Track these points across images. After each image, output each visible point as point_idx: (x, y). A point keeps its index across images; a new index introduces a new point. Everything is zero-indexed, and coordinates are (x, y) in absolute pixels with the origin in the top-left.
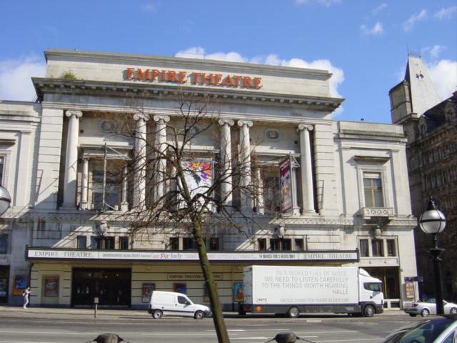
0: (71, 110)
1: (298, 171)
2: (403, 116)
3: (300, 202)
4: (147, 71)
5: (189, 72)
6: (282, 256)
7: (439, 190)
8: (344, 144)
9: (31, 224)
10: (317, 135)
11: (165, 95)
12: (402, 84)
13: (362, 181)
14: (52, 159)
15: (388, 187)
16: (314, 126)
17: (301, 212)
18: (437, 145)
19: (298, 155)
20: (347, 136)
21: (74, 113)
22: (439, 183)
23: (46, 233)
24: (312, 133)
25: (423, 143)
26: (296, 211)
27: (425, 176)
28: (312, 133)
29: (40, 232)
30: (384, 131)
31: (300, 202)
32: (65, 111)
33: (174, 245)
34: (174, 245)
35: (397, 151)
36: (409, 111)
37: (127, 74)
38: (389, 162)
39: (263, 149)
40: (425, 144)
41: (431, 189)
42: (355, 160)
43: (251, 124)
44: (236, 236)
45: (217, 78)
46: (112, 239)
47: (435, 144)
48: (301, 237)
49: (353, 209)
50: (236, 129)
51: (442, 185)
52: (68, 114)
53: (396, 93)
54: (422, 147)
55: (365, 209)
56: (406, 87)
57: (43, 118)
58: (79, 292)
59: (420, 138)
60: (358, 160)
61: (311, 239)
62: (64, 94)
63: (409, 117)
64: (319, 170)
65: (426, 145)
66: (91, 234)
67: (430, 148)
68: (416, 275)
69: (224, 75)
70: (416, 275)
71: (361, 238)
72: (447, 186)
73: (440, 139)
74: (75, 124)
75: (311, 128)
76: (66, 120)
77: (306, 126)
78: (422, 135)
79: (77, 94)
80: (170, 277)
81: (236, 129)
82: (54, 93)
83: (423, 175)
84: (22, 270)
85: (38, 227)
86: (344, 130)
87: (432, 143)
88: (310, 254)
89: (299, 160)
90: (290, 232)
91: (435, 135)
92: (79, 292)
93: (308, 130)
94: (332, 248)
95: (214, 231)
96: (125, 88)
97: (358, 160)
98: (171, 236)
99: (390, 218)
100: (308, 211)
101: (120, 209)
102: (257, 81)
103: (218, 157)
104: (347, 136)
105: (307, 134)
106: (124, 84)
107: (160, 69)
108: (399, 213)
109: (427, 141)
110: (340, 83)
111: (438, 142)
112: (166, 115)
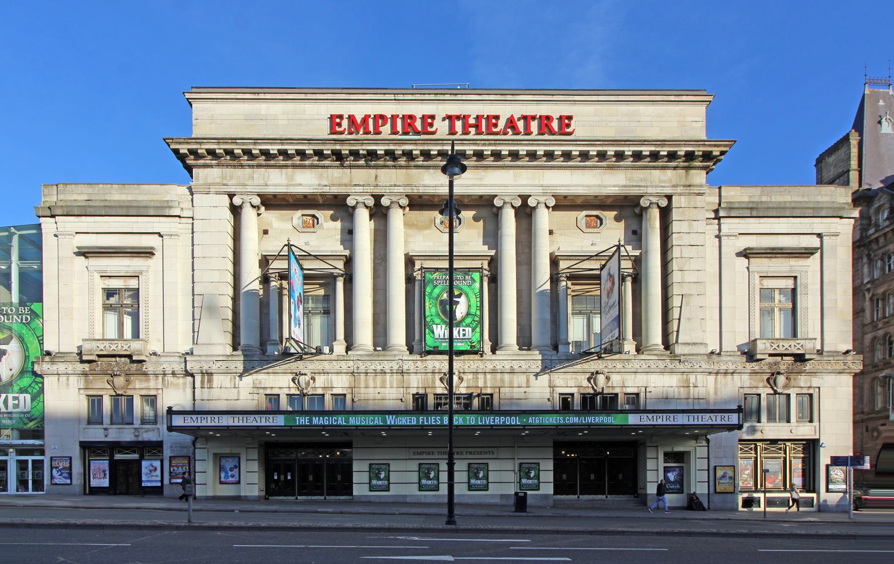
0: (242, 193)
3: (638, 333)
4: (366, 119)
8: (728, 226)
10: (675, 215)
12: (846, 139)
13: (757, 297)
15: (809, 303)
16: (669, 198)
21: (247, 198)
24: (665, 213)
25: (877, 239)
29: (206, 390)
31: (638, 333)
35: (836, 235)
38: (818, 255)
40: (882, 240)
41: (884, 317)
43: (552, 202)
44: (523, 390)
49: (736, 337)
52: (237, 201)
54: (874, 246)
55: (758, 342)
57: (196, 210)
58: (276, 478)
66: (287, 391)
75: (664, 203)
76: (236, 211)
77: (654, 200)
78: (877, 225)
80: (414, 453)
83: (868, 296)
84: (182, 447)
85: (202, 382)
88: (650, 416)
92: (276, 478)
93: (659, 207)
97: (84, 253)
98: (414, 391)
99: (807, 357)
100: (649, 350)
101: (331, 350)
105: (655, 214)
108: (825, 349)
109: (885, 235)
110: (828, 503)
112: (401, 194)
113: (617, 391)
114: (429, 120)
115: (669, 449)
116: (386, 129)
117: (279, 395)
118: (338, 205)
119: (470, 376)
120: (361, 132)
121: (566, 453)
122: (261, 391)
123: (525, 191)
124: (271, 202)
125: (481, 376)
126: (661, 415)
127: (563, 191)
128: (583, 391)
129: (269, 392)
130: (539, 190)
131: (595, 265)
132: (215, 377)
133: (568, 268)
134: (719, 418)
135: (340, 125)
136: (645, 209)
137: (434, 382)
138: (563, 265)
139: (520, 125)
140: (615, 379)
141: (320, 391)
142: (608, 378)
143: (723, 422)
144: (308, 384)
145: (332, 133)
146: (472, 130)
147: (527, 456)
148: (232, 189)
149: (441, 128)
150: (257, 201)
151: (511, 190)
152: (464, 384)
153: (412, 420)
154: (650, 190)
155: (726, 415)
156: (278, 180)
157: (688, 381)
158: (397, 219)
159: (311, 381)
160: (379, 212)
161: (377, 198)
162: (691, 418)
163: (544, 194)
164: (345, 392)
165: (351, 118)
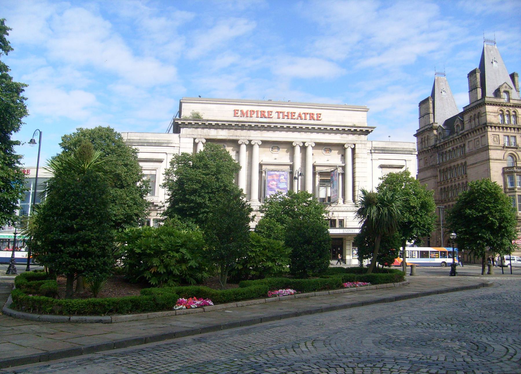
1: (344, 175)
2: (427, 124)
5: (275, 109)
7: (448, 182)
10: (357, 151)
12: (427, 100)
16: (355, 145)
17: (344, 202)
18: (448, 149)
19: (343, 165)
21: (200, 140)
22: (449, 177)
24: (353, 150)
26: (341, 201)
27: (440, 171)
28: (353, 150)
30: (402, 147)
32: (194, 139)
36: (432, 120)
37: (236, 112)
45: (293, 114)
46: (335, 220)
47: (447, 148)
50: (304, 148)
51: (451, 178)
52: (197, 141)
53: (424, 106)
56: (431, 102)
59: (438, 142)
63: (431, 126)
64: (357, 175)
65: (441, 149)
67: (444, 151)
69: (297, 111)
72: (453, 180)
73: (450, 145)
75: (353, 147)
81: (304, 148)
83: (438, 170)
86: (374, 147)
87: (446, 147)
89: (344, 168)
90: (336, 214)
91: (456, 138)
94: (361, 300)
102: (319, 115)
103: (292, 167)
104: (376, 152)
107: (255, 108)
111: (449, 147)
114: (270, 113)
116: (255, 115)
130: (309, 140)
136: (239, 146)
139: (303, 116)
142: (333, 214)
148: (195, 137)
149: (275, 115)
154: (242, 138)
158: (256, 149)
160: (250, 147)
163: (311, 142)
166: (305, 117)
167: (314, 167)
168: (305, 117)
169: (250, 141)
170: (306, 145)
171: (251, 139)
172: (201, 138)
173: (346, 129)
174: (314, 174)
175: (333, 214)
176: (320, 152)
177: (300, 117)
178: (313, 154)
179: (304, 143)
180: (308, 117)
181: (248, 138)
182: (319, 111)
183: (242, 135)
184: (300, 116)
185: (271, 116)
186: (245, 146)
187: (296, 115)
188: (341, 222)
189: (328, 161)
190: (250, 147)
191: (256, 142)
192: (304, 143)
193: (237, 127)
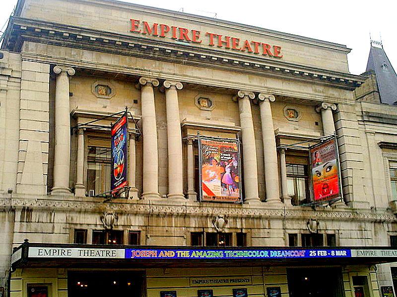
4: (155, 25)
6: (235, 254)
9: (11, 214)
11: (178, 57)
14: (39, 126)
20: (371, 119)
23: (33, 226)
26: (134, 195)
33: (80, 238)
34: (80, 238)
37: (134, 24)
39: (288, 128)
42: (381, 147)
44: (266, 231)
46: (121, 233)
48: (332, 232)
52: (57, 70)
60: (384, 146)
61: (344, 234)
62: (52, 43)
66: (93, 227)
68: (29, 257)
70: (29, 257)
71: (391, 234)
74: (63, 83)
76: (54, 78)
79: (68, 46)
81: (256, 103)
82: (39, 41)
85: (22, 217)
95: (242, 224)
96: (132, 43)
97: (384, 146)
98: (193, 230)
104: (371, 119)
106: (131, 38)
113: (323, 232)
115: (355, 275)
117: (87, 230)
118: (233, 96)
119: (231, 220)
120: (151, 35)
121: (81, 284)
122: (73, 226)
123: (257, 90)
124: (83, 74)
125: (239, 220)
126: (57, 249)
127: (279, 93)
128: (302, 232)
129: (78, 227)
131: (108, 124)
132: (33, 214)
133: (86, 124)
134: (105, 253)
135: (137, 27)
136: (239, 99)
137: (207, 224)
138: (81, 121)
139: (252, 48)
140: (322, 225)
141: (121, 228)
142: (318, 224)
143: (63, 256)
144: (112, 222)
145: (132, 32)
146: (224, 46)
147: (273, 282)
150: (273, 99)
151: (247, 88)
152: (227, 226)
153: (289, 254)
154: (147, 73)
155: (66, 249)
156: (89, 59)
157: (360, 226)
158: (172, 98)
159: (115, 220)
160: (256, 103)
161: (162, 81)
162: (82, 253)
163: (268, 93)
164: (140, 229)
165: (145, 24)
166: (256, 49)
167: (74, 117)
168: (256, 49)
169: (162, 81)
170: (166, 84)
171: (163, 76)
172: (65, 65)
173: (334, 77)
174: (185, 143)
175: (318, 224)
176: (85, 88)
177: (247, 48)
178: (71, 95)
179: (257, 94)
180: (260, 50)
181: (156, 75)
182: (277, 44)
183: (150, 69)
184: (247, 46)
185: (279, 55)
186: (248, 101)
187: (241, 45)
188: (331, 237)
189: (105, 107)
190: (161, 91)
191: (173, 84)
192: (257, 94)
193: (70, 42)
